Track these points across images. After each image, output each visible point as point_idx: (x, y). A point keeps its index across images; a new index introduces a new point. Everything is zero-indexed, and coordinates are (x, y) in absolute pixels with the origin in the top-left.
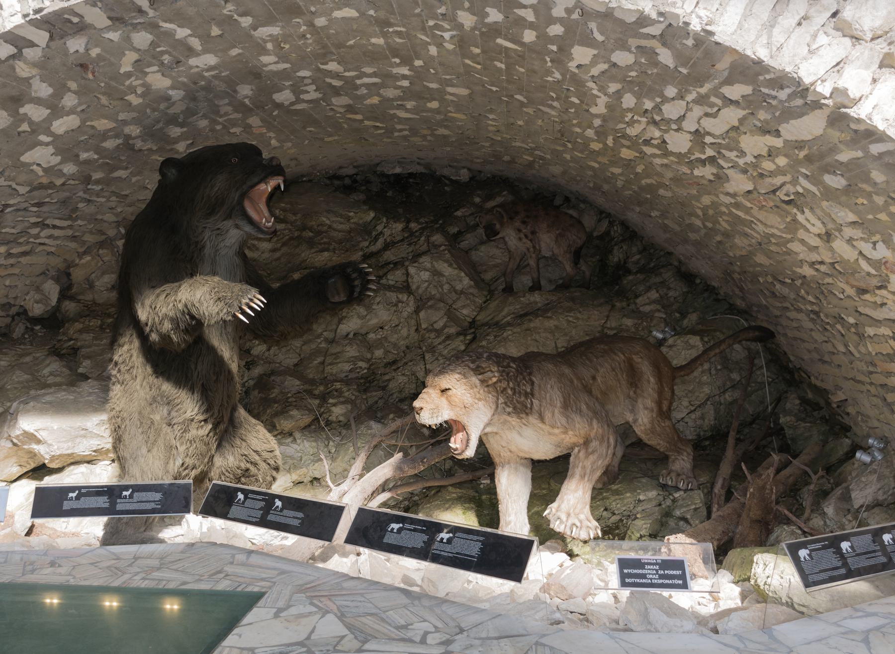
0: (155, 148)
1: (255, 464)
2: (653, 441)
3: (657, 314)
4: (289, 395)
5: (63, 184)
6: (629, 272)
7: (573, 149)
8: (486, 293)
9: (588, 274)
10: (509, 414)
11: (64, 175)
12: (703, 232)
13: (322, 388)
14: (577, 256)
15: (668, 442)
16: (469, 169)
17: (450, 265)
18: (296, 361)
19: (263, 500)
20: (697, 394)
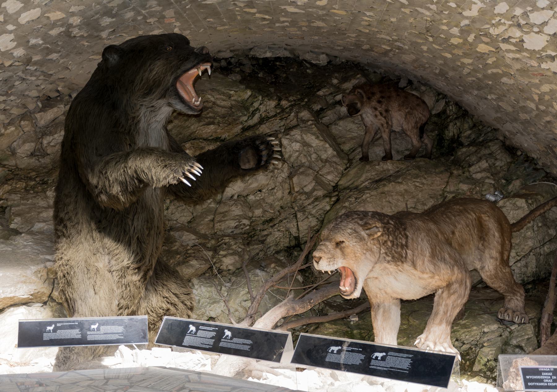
0: (85, 35)
1: (174, 305)
2: (496, 285)
3: (487, 181)
4: (189, 248)
5: (11, 66)
6: (461, 145)
7: (433, 42)
8: (346, 161)
9: (429, 146)
10: (388, 262)
11: (14, 57)
12: (534, 113)
13: (213, 242)
14: (422, 130)
15: (507, 285)
16: (327, 55)
17: (317, 138)
18: (189, 219)
19: (213, 331)
20: (522, 246)
